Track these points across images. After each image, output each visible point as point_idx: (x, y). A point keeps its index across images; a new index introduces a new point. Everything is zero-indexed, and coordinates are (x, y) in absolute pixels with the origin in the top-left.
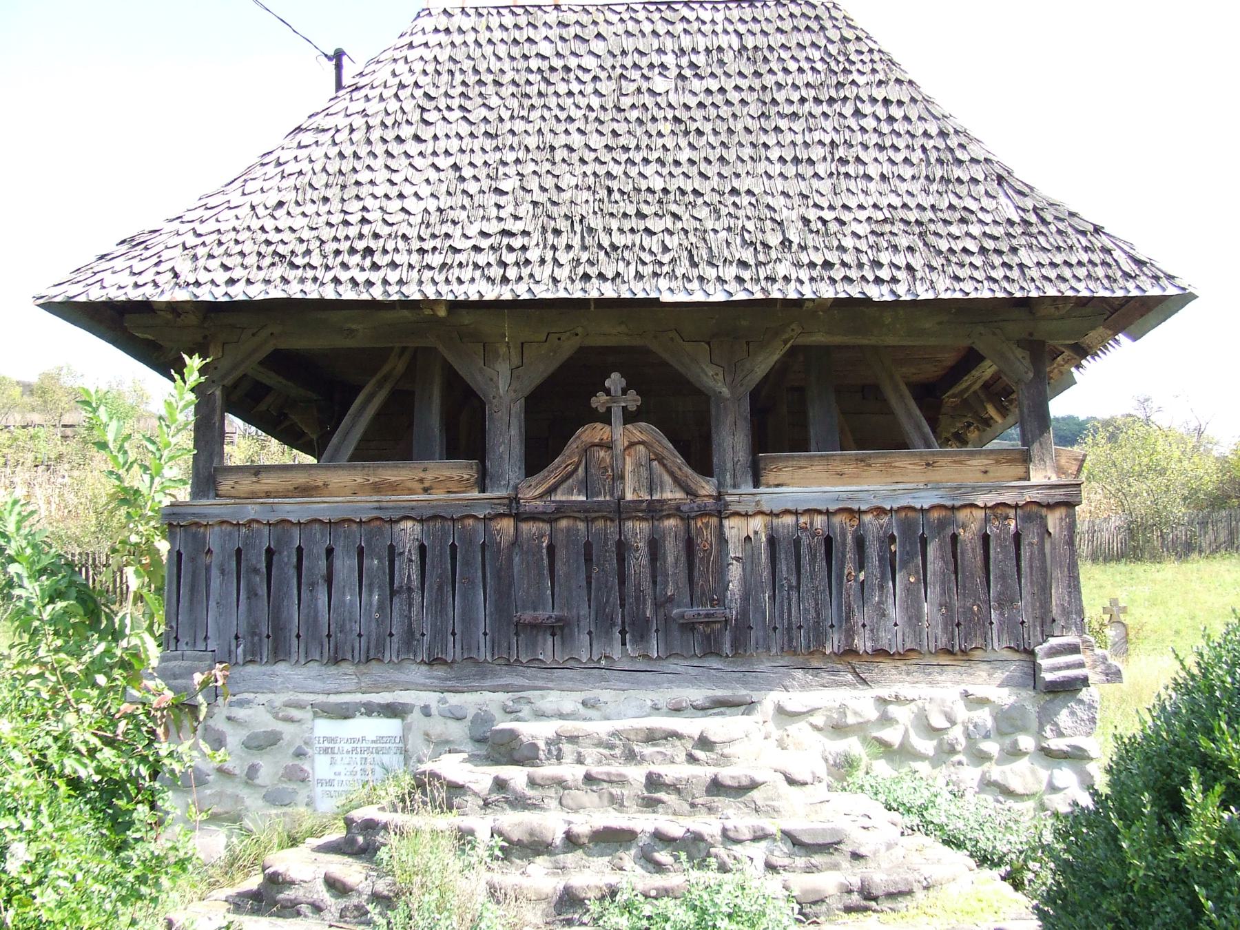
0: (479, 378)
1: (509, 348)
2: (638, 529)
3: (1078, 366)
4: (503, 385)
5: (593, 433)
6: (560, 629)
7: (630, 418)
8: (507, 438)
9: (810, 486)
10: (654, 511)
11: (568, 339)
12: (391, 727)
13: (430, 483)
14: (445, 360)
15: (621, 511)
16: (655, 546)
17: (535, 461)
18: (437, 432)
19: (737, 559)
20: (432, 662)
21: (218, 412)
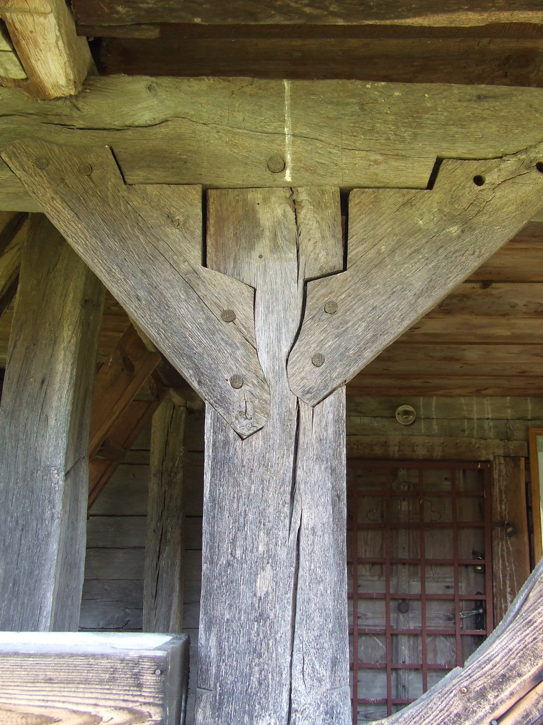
0: (184, 309)
1: (295, 205)
4: (270, 331)
11: (512, 178)
14: (94, 283)
18: (58, 478)
19: (58, 518)
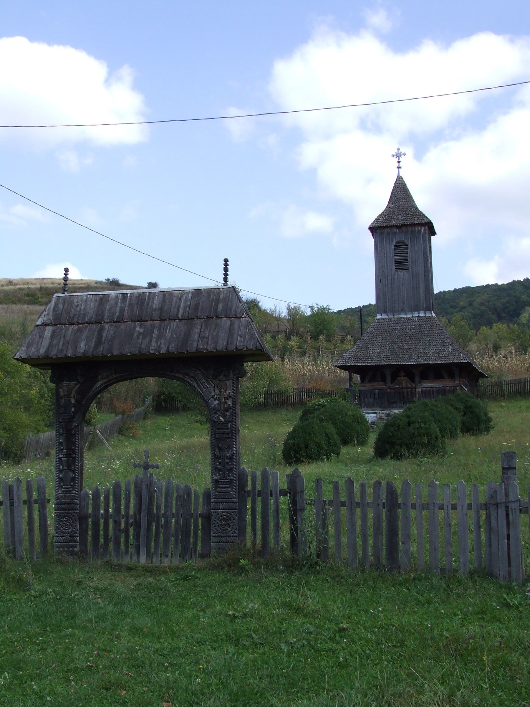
2: (405, 390)
3: (343, 446)
5: (399, 378)
6: (396, 402)
7: (404, 376)
8: (389, 379)
9: (426, 385)
10: (407, 388)
12: (375, 415)
13: (378, 385)
15: (403, 388)
16: (407, 392)
17: (393, 381)
20: (380, 407)
21: (427, 236)
